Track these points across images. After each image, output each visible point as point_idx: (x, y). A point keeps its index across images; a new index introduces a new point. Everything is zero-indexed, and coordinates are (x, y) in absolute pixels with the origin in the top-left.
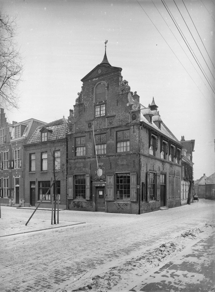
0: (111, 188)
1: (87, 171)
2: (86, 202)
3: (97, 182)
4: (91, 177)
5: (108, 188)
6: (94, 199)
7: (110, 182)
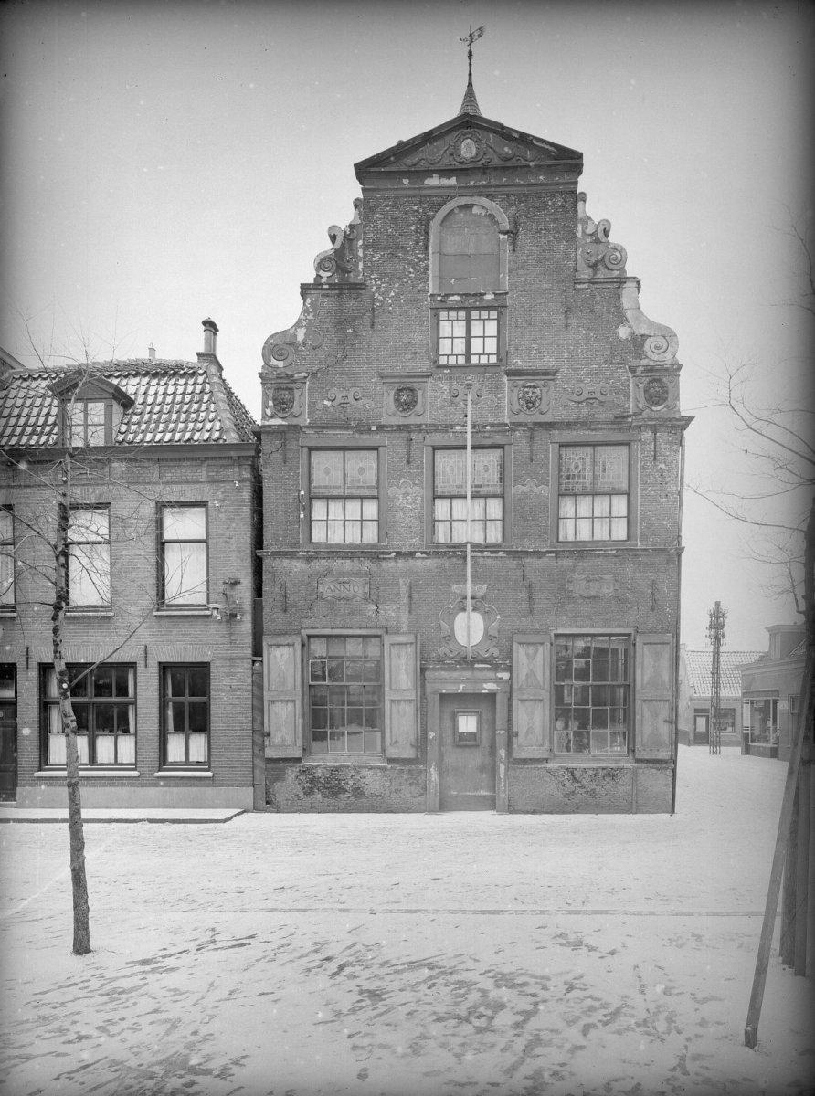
2: (383, 769)
3: (455, 674)
5: (522, 700)
6: (432, 751)
7: (531, 674)
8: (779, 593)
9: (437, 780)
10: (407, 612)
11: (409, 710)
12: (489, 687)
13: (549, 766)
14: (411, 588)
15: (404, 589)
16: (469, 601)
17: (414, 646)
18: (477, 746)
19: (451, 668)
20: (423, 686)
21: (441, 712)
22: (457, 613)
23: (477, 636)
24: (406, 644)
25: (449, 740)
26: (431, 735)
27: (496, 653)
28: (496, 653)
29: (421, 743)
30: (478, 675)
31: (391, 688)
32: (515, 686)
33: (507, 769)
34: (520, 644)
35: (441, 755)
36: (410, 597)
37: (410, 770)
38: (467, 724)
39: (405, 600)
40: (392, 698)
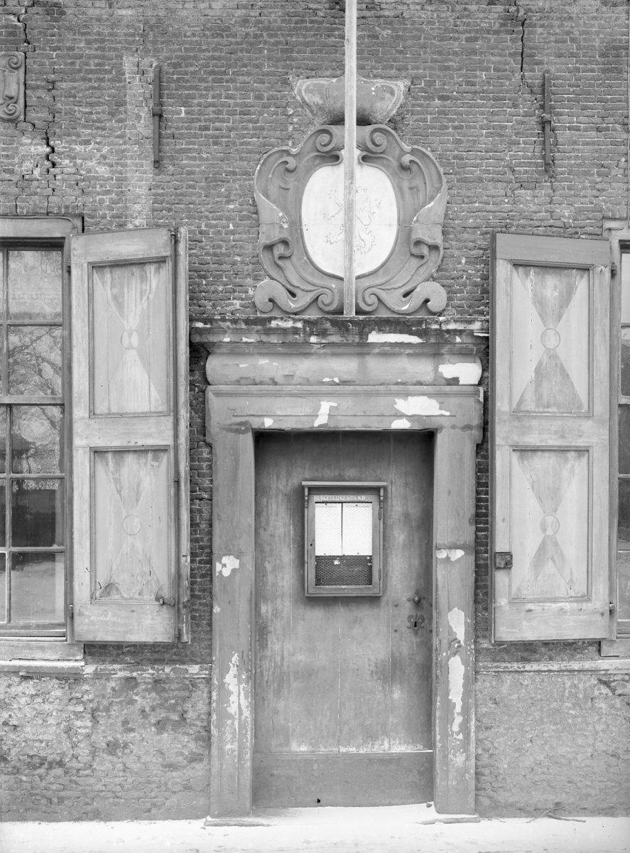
0: (563, 450)
1: (83, 183)
2: (70, 678)
3: (303, 367)
4: (197, 273)
5: (524, 451)
6: (230, 616)
7: (550, 369)
8: (290, 639)
9: (247, 713)
10: (148, 165)
11: (151, 481)
12: (412, 410)
13: (603, 664)
14: (160, 88)
15: (137, 89)
16: (350, 133)
17: (168, 266)
18: (374, 600)
19: (293, 347)
20: (199, 406)
21: (260, 490)
22: (309, 171)
23: (377, 241)
24: (141, 263)
25: (285, 580)
26: (226, 566)
27: (438, 297)
28: (438, 297)
29: (194, 594)
30: (377, 367)
31: (92, 413)
32: (502, 406)
33: (473, 676)
34: (516, 265)
35: (260, 632)
36: (158, 116)
37: (157, 682)
38: (344, 529)
39: (143, 125)
40: (99, 442)
